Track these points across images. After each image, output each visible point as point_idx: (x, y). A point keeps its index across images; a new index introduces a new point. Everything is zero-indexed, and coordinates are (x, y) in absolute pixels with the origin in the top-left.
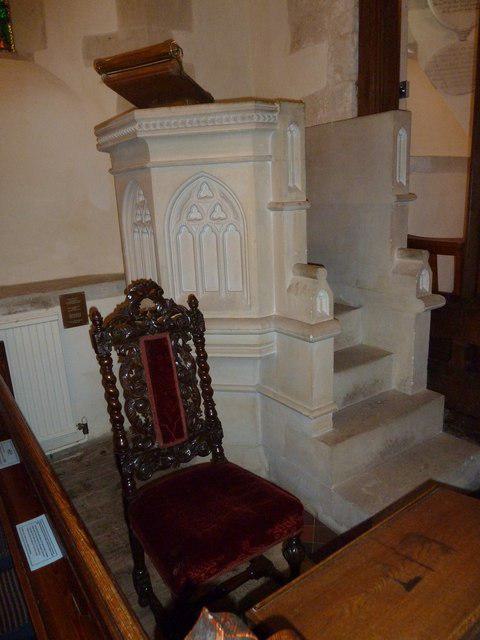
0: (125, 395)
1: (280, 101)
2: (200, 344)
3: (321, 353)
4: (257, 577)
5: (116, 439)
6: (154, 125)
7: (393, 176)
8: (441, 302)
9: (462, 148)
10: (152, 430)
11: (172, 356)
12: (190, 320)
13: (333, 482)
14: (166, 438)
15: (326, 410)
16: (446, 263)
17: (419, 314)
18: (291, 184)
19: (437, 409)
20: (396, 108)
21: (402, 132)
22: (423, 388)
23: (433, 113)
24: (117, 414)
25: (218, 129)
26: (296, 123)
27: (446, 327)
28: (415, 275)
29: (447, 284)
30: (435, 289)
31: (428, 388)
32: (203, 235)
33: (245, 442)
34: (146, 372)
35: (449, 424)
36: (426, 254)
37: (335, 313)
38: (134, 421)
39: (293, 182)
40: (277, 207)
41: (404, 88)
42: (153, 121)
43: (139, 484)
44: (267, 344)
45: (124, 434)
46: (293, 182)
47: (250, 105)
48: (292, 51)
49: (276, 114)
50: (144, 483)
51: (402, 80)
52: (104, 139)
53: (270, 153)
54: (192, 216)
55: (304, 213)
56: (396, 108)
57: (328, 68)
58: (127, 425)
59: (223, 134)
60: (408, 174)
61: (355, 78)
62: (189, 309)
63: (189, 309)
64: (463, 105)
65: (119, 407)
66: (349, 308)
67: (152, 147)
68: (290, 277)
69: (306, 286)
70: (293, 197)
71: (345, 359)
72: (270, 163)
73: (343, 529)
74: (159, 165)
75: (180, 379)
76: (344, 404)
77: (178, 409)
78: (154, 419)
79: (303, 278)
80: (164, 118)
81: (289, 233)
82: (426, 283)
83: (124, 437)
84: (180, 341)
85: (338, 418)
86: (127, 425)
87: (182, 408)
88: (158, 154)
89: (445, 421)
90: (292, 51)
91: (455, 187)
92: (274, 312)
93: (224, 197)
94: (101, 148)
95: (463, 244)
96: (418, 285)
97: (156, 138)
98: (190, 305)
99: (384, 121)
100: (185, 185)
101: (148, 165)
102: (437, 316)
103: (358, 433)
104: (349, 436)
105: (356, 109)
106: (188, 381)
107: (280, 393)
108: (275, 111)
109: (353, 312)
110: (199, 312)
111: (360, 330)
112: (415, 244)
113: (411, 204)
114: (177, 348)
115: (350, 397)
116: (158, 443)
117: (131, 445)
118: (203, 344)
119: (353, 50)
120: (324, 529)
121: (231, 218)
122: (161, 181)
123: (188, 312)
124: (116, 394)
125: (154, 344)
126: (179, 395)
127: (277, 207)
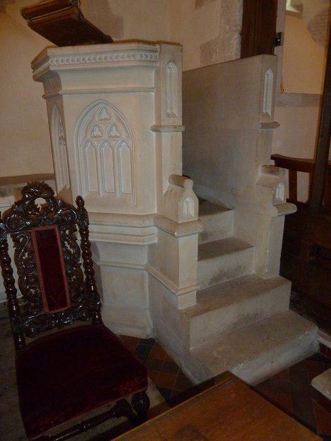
0: (19, 273)
1: (159, 43)
2: (85, 233)
3: (188, 245)
4: (118, 416)
5: (10, 306)
6: (67, 60)
7: (260, 108)
8: (293, 209)
9: (317, 89)
10: (41, 300)
11: (60, 244)
12: (77, 215)
13: (202, 340)
14: (52, 307)
15: (190, 290)
16: (303, 178)
17: (274, 218)
18: (169, 111)
19: (285, 291)
20: (271, 53)
21: (269, 72)
22: (276, 274)
23: (299, 57)
24: (11, 287)
25: (110, 65)
26: (174, 61)
27: (297, 231)
28: (272, 187)
29: (303, 195)
30: (292, 198)
31: (281, 274)
32: (121, 149)
33: (126, 307)
34: (37, 254)
35: (295, 304)
36: (286, 173)
37: (199, 216)
38: (26, 296)
39: (172, 109)
40: (157, 129)
41: (280, 38)
42: (64, 58)
43: (29, 340)
44: (148, 235)
45: (17, 302)
46: (172, 109)
47: (134, 45)
48: (196, 8)
49: (157, 54)
50: (33, 339)
51: (278, 31)
52: (36, 72)
53: (153, 86)
54: (95, 133)
55: (180, 135)
56: (271, 53)
57: (223, 23)
58: (19, 295)
59: (114, 68)
60: (273, 106)
61: (239, 28)
62: (76, 207)
63: (76, 207)
64: (321, 52)
65: (13, 281)
66: (221, 208)
67: (64, 79)
68: (167, 185)
69: (176, 193)
70: (171, 121)
71: (208, 250)
72: (153, 93)
73: (197, 382)
74: (70, 93)
75: (65, 260)
76: (210, 283)
77: (63, 286)
78: (41, 291)
79: (176, 186)
80: (68, 55)
81: (171, 146)
82: (282, 193)
83: (16, 305)
84: (67, 232)
85: (201, 295)
86: (19, 295)
87: (66, 284)
88: (67, 84)
89: (291, 301)
90: (196, 8)
91: (312, 115)
92: (155, 211)
93: (119, 119)
94: (37, 79)
95: (315, 164)
96: (274, 195)
97: (66, 71)
98: (78, 203)
99: (257, 61)
100: (87, 109)
101: (60, 93)
102: (289, 219)
103: (215, 308)
104: (206, 311)
105: (240, 54)
106: (73, 262)
107: (159, 273)
108: (156, 51)
109: (226, 213)
110: (84, 210)
111: (226, 225)
112: (280, 162)
113: (275, 131)
114: (64, 237)
115: (216, 278)
116: (46, 309)
117: (22, 311)
118: (87, 235)
119: (238, 6)
120: (183, 378)
121: (124, 135)
122: (70, 104)
123: (75, 210)
124: (11, 271)
125: (52, 231)
126: (64, 274)
127: (157, 129)
